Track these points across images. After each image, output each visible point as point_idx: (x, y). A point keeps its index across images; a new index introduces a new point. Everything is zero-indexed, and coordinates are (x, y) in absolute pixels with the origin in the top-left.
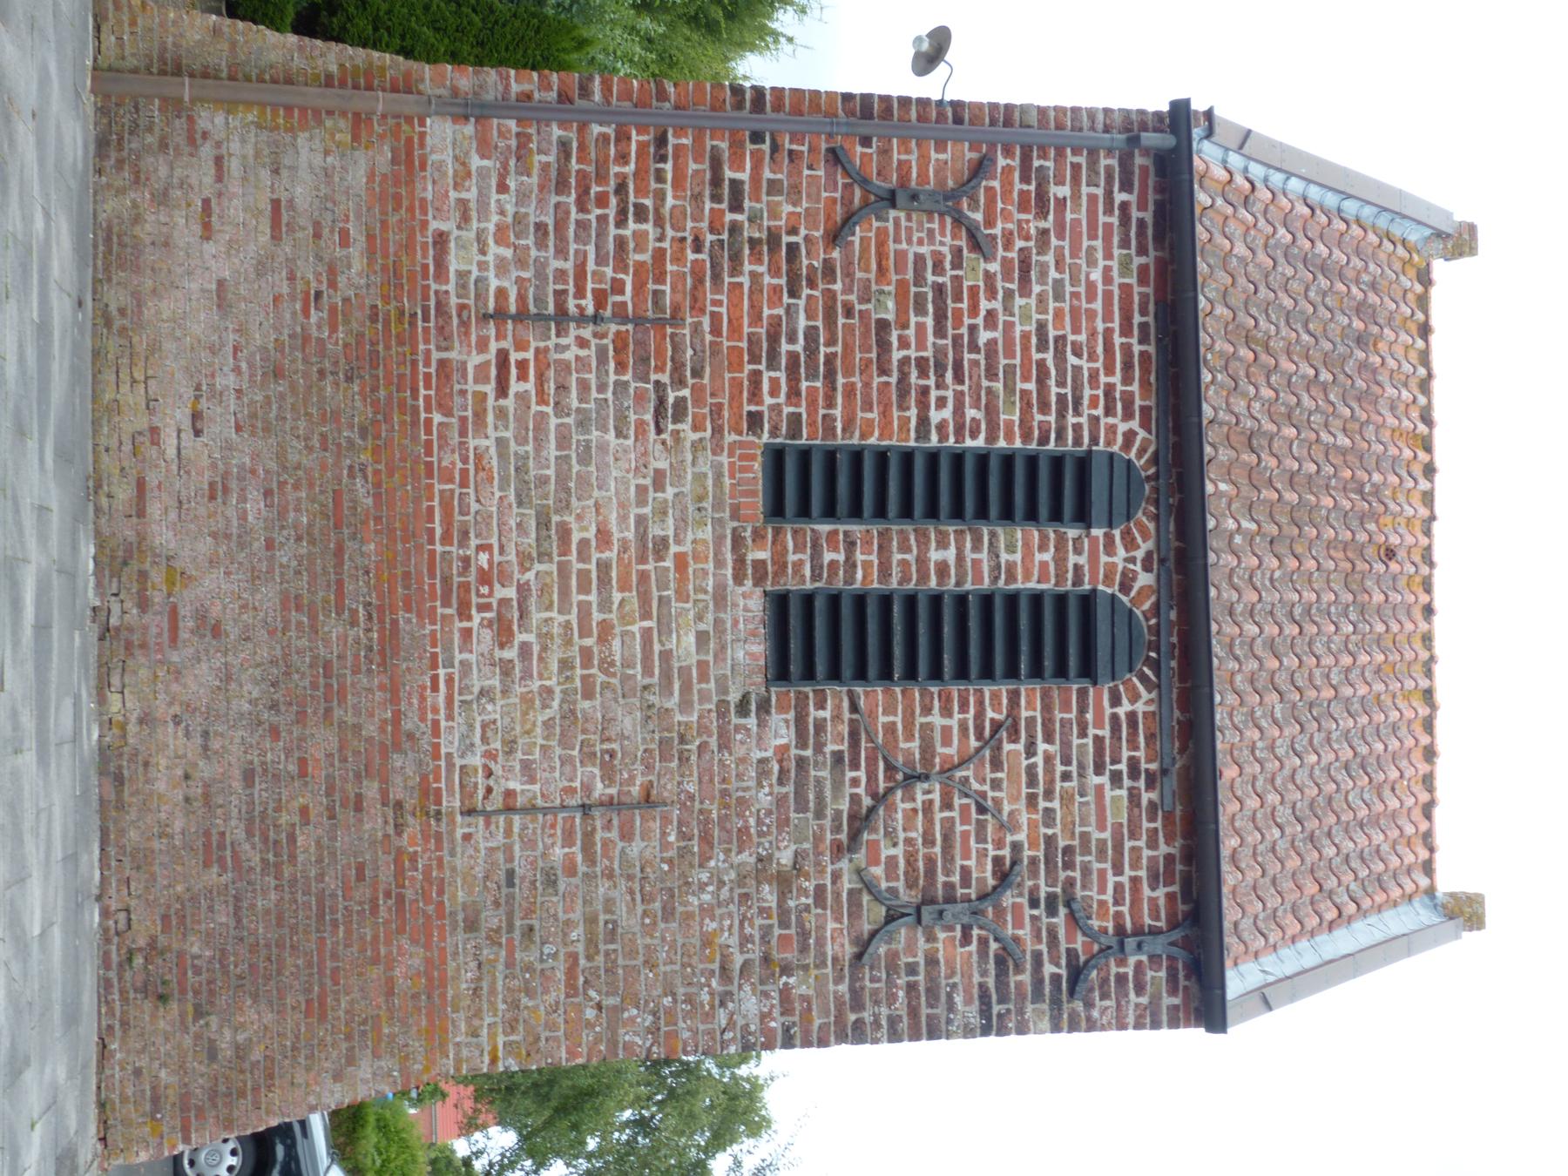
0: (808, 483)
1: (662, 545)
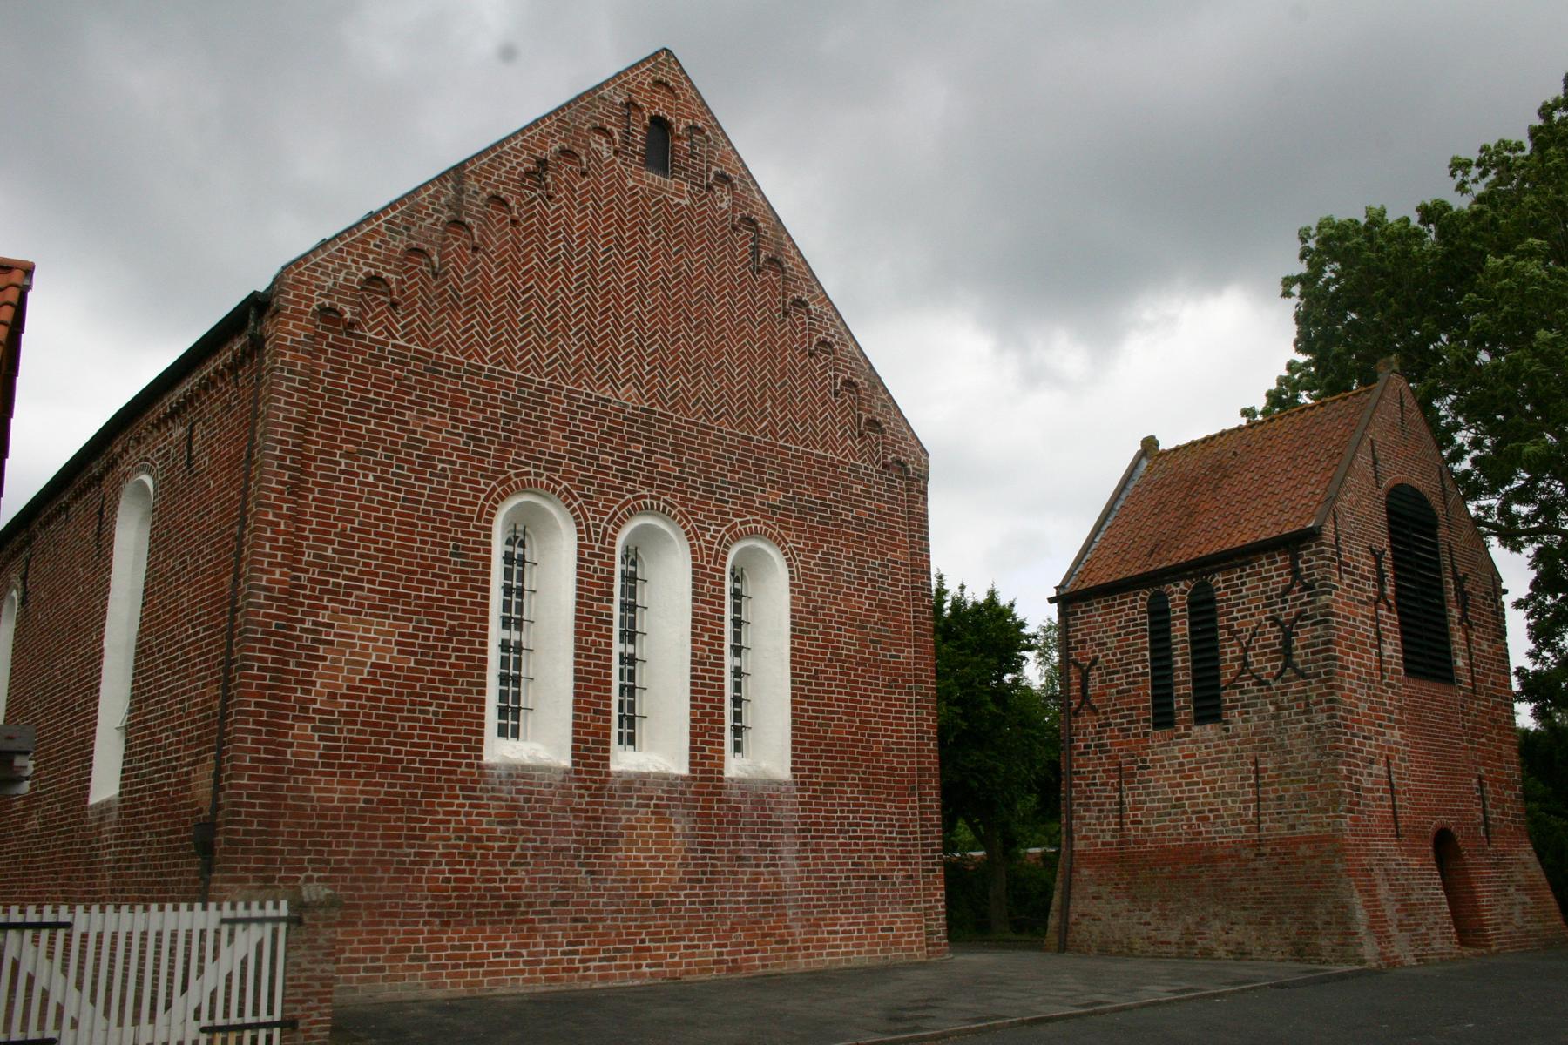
0: (1163, 717)
1: (1181, 764)
